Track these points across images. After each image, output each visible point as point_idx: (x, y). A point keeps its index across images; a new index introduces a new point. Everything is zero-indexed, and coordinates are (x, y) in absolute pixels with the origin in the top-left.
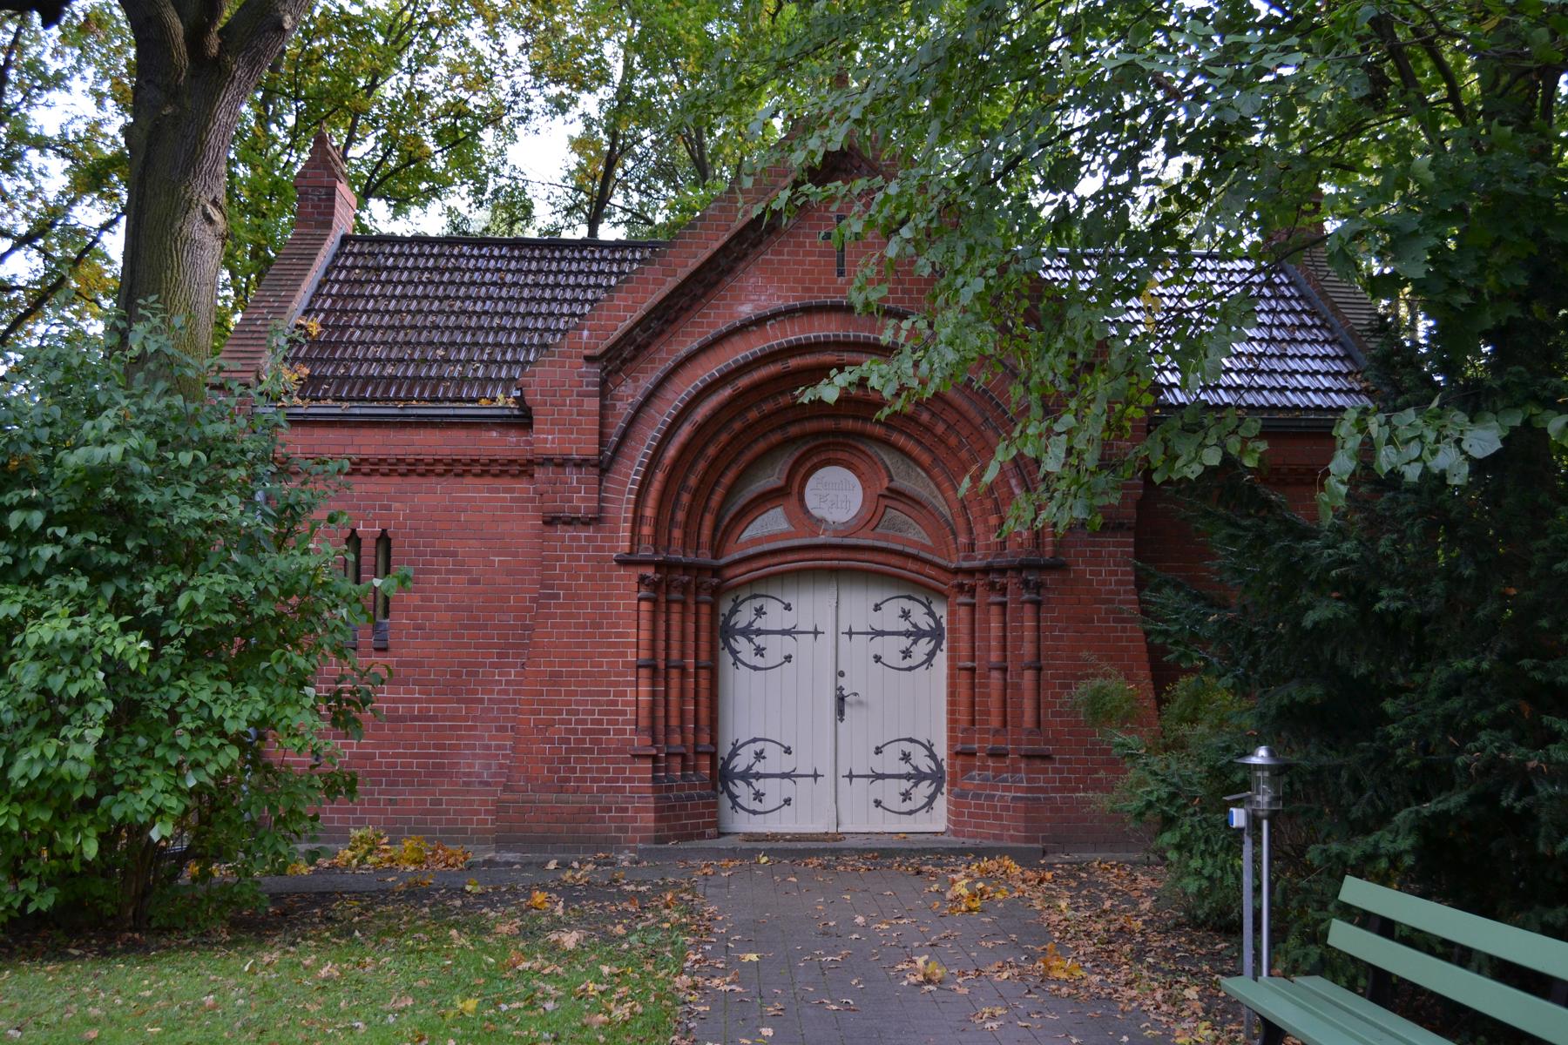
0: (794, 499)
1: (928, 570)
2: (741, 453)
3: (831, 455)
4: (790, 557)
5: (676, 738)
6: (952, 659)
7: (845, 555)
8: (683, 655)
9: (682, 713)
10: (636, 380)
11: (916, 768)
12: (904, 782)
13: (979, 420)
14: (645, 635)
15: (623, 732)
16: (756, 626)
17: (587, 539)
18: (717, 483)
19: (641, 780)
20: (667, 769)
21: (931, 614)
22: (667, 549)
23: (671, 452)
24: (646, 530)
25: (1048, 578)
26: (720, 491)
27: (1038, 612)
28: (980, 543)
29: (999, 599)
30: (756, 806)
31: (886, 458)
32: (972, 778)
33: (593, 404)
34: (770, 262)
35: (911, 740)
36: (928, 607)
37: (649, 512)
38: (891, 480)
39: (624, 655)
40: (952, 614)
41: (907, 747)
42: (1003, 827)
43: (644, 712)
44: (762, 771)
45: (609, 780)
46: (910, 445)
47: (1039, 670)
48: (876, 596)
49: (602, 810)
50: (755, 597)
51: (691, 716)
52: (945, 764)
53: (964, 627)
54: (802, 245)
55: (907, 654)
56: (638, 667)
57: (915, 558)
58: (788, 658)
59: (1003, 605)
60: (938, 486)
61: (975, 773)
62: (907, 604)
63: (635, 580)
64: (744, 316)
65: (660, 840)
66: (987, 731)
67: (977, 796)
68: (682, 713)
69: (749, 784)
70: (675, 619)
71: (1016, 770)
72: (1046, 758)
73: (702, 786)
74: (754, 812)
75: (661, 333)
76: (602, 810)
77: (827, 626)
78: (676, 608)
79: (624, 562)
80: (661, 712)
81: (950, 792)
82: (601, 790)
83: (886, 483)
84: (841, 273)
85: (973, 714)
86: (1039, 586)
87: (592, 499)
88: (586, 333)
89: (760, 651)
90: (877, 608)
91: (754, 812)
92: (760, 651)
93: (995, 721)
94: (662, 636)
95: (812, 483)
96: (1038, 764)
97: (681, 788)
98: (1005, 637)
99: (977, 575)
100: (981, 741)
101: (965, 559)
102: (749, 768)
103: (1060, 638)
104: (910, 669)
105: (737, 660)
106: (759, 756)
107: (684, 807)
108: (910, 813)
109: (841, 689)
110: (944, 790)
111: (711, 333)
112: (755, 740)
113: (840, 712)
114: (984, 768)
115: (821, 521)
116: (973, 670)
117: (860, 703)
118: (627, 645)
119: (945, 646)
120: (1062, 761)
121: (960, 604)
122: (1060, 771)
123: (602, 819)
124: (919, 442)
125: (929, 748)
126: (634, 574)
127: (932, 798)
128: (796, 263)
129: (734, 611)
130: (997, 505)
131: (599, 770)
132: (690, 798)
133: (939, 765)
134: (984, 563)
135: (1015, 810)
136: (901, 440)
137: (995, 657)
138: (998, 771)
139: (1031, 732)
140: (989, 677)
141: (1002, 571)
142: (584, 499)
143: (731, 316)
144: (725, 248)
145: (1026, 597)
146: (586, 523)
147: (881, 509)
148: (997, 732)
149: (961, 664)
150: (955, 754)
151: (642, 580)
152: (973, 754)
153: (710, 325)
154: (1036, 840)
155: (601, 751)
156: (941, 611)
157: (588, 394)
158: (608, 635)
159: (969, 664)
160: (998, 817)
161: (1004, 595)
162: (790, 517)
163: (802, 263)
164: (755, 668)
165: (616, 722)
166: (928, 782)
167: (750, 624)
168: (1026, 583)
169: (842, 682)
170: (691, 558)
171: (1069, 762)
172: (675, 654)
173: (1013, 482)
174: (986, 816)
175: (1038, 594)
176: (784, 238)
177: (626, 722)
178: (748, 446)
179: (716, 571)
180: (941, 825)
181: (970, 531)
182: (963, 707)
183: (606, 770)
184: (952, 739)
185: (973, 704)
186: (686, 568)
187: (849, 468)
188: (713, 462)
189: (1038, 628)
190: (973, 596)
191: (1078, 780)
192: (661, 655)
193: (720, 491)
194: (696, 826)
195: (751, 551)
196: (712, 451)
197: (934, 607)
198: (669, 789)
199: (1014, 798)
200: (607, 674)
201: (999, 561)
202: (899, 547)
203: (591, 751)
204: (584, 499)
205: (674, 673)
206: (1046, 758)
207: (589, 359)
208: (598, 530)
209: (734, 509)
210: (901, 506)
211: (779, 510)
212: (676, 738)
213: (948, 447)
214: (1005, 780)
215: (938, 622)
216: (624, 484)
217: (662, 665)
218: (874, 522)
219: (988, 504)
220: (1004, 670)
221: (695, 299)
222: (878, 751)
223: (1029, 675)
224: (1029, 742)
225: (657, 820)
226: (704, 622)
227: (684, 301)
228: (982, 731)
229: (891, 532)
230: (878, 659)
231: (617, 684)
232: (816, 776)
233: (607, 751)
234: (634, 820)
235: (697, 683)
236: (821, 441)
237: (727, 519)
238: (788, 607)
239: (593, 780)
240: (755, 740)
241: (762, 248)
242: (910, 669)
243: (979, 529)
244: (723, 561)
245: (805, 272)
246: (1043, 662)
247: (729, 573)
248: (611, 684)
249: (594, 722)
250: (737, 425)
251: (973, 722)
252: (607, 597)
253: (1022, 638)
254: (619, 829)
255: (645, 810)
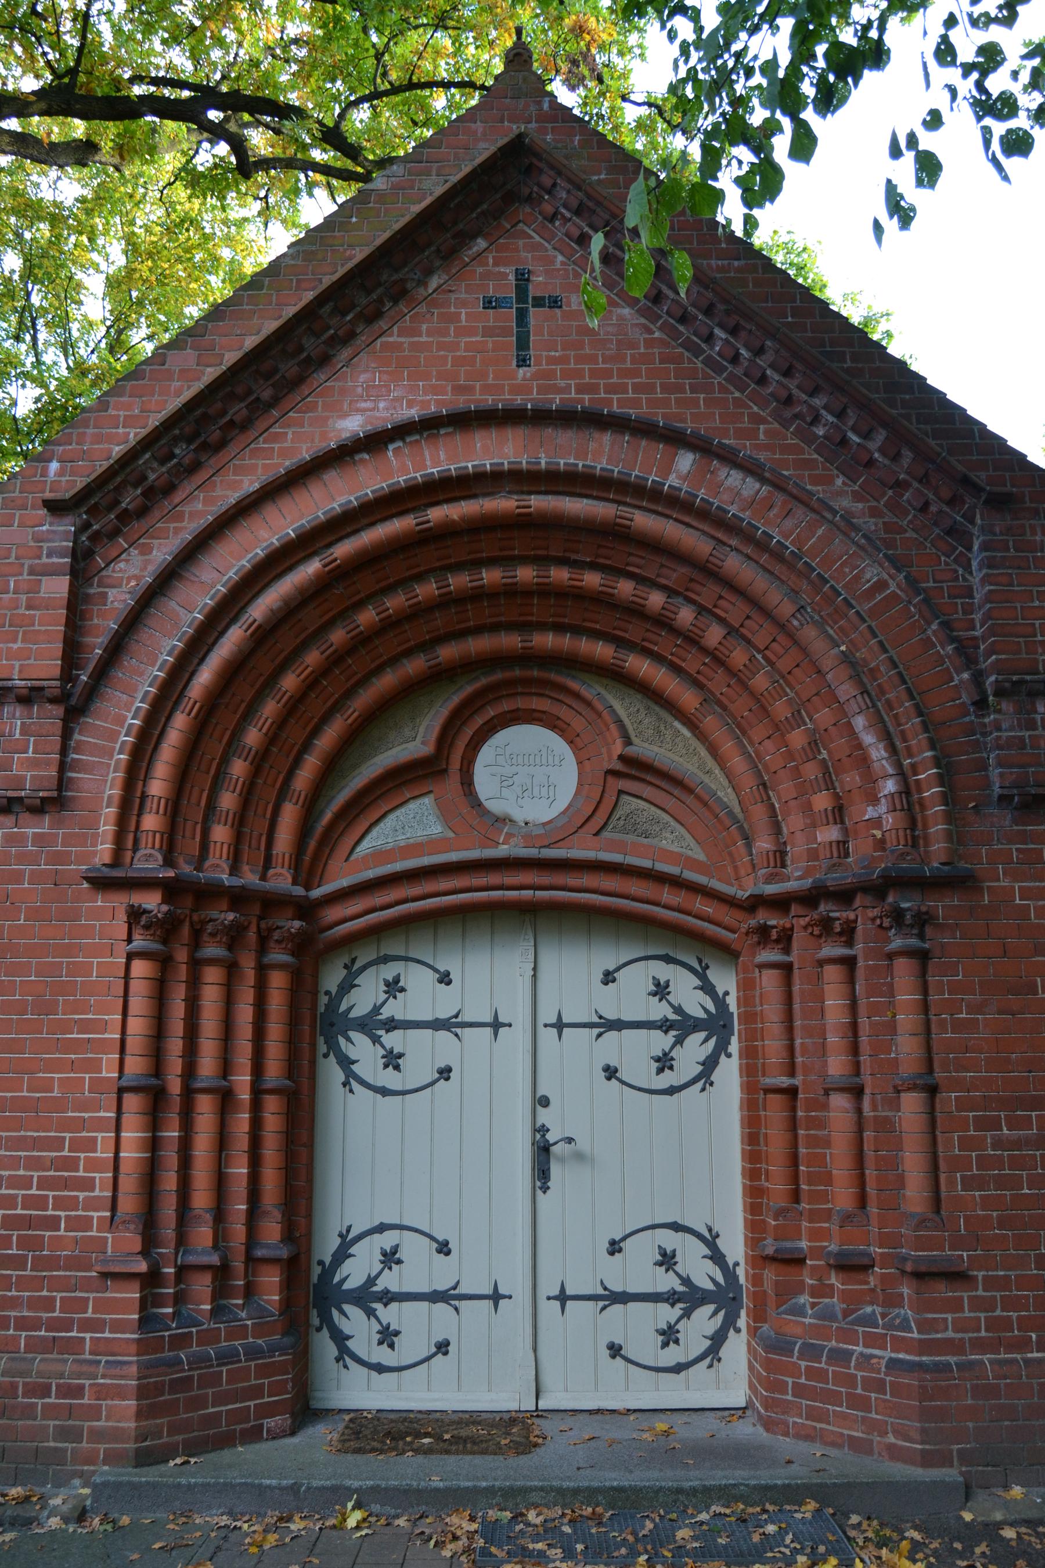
0: (453, 782)
1: (700, 904)
2: (349, 694)
3: (520, 703)
4: (444, 884)
5: (203, 1234)
6: (750, 1071)
7: (546, 879)
8: (226, 1068)
9: (221, 1182)
10: (146, 550)
11: (686, 1281)
12: (663, 1308)
13: (787, 609)
14: (137, 1026)
15: (85, 1223)
16: (386, 1013)
17: (38, 839)
18: (306, 746)
19: (117, 1326)
20: (179, 1299)
21: (707, 988)
22: (199, 865)
23: (205, 676)
24: (151, 822)
25: (940, 905)
26: (311, 763)
27: (923, 973)
28: (796, 849)
29: (840, 951)
30: (383, 1355)
31: (617, 706)
32: (800, 1311)
33: (58, 587)
34: (398, 346)
35: (676, 1227)
36: (702, 976)
37: (158, 787)
38: (628, 742)
39: (94, 1066)
40: (746, 986)
41: (669, 1240)
42: (872, 1426)
43: (129, 1183)
44: (394, 1288)
45: (54, 1325)
46: (659, 676)
47: (932, 1091)
48: (607, 957)
49: (32, 1391)
50: (386, 959)
51: (239, 1187)
52: (741, 1272)
53: (772, 1011)
54: (455, 318)
55: (664, 1062)
56: (121, 1091)
57: (676, 882)
58: (445, 1073)
59: (849, 963)
60: (713, 750)
61: (804, 1299)
62: (663, 971)
63: (122, 917)
64: (345, 435)
65: (145, 1458)
66: (828, 1215)
67: (811, 1352)
68: (221, 1182)
69: (371, 1313)
70: (211, 996)
71: (893, 1301)
72: (957, 1277)
73: (260, 1330)
74: (380, 1368)
75: (194, 467)
76: (32, 1391)
77: (517, 1012)
78: (212, 975)
79: (101, 883)
80: (169, 1181)
81: (753, 1332)
82: (33, 1346)
83: (618, 748)
84: (522, 362)
85: (795, 1178)
86: (923, 921)
87: (48, 762)
88: (54, 466)
89: (393, 1060)
90: (608, 978)
91: (380, 1368)
92: (393, 1060)
93: (843, 1197)
94: (177, 1026)
95: (486, 754)
96: (942, 1291)
97: (209, 1337)
98: (854, 1026)
99: (795, 909)
100: (816, 1235)
101: (769, 879)
102: (371, 1281)
103: (970, 1025)
104: (671, 1091)
105: (351, 1077)
106: (390, 1258)
107: (206, 1381)
108: (678, 1368)
109: (544, 1130)
110: (742, 1322)
111: (284, 465)
112: (381, 1228)
113: (542, 1174)
114: (822, 1291)
115: (504, 820)
116: (792, 1092)
117: (579, 1157)
118: (101, 1046)
119: (734, 1047)
120: (990, 1283)
121: (762, 966)
122: (986, 1305)
123: (28, 1411)
124: (676, 669)
125: (711, 1241)
126: (119, 902)
127: (718, 1340)
128: (441, 346)
129: (347, 986)
130: (826, 772)
131: (35, 1304)
132: (227, 1357)
133: (729, 1273)
134: (808, 882)
135: (897, 1390)
136: (641, 666)
137: (836, 1066)
138: (853, 1300)
139: (922, 1223)
140: (825, 1107)
141: (844, 896)
142: (34, 764)
143: (324, 436)
144: (307, 315)
145: (897, 943)
146: (39, 808)
147: (610, 798)
148: (847, 1219)
149: (769, 1081)
150: (759, 1260)
151: (135, 915)
152: (799, 1261)
153: (284, 453)
154: (942, 1459)
155: (40, 1263)
156: (726, 981)
157: (51, 571)
158: (65, 1027)
159: (784, 1081)
160: (861, 1403)
161: (850, 943)
162: (445, 813)
163: (454, 347)
164: (384, 1092)
165: (72, 1204)
166: (709, 1309)
167: (377, 1009)
168: (898, 916)
169: (544, 1116)
170: (250, 878)
171: (1003, 1284)
172: (207, 1066)
173: (859, 722)
174: (833, 1397)
175: (921, 936)
176: (422, 309)
177: (91, 1204)
178: (364, 681)
179: (306, 910)
180: (737, 1395)
181: (776, 828)
182: (776, 1167)
183: (48, 1304)
184: (755, 1229)
185: (794, 1160)
186: (238, 898)
187: (553, 727)
188: (293, 707)
189: (925, 1007)
190: (787, 951)
191: (1025, 1324)
192: (175, 1065)
193: (311, 763)
194: (242, 1415)
195: (371, 874)
196: (290, 682)
197: (712, 975)
198: (180, 1341)
199: (893, 1363)
200: (59, 1105)
201: (835, 879)
202: (647, 863)
203: (18, 1262)
204: (34, 764)
205: (205, 1107)
206: (957, 1277)
207: (55, 507)
208: (57, 824)
209: (342, 797)
210: (647, 791)
211: (427, 800)
212: (203, 1234)
213: (731, 672)
214: (869, 1321)
215: (720, 1002)
216: (113, 736)
217: (175, 1086)
218: (599, 820)
219: (811, 771)
220: (857, 1092)
221: (259, 408)
222: (614, 1248)
223: (912, 1103)
224: (921, 1244)
225: (140, 1415)
226: (277, 1003)
227: (237, 410)
228: (814, 1216)
229: (631, 838)
230: (611, 1072)
231: (81, 1124)
232: (496, 1297)
233: (52, 1263)
234: (94, 1413)
235: (256, 1123)
236: (499, 676)
237: (328, 816)
238: (445, 979)
239: (22, 1324)
240: (381, 1228)
241: (383, 324)
242: (671, 1091)
243: (793, 823)
244: (316, 893)
245: (458, 362)
246: (939, 1075)
247: (333, 914)
248: (66, 1125)
249: (30, 1202)
250: (338, 636)
251: (796, 1196)
252: (68, 951)
253: (892, 1027)
254: (64, 1434)
255: (119, 1393)
